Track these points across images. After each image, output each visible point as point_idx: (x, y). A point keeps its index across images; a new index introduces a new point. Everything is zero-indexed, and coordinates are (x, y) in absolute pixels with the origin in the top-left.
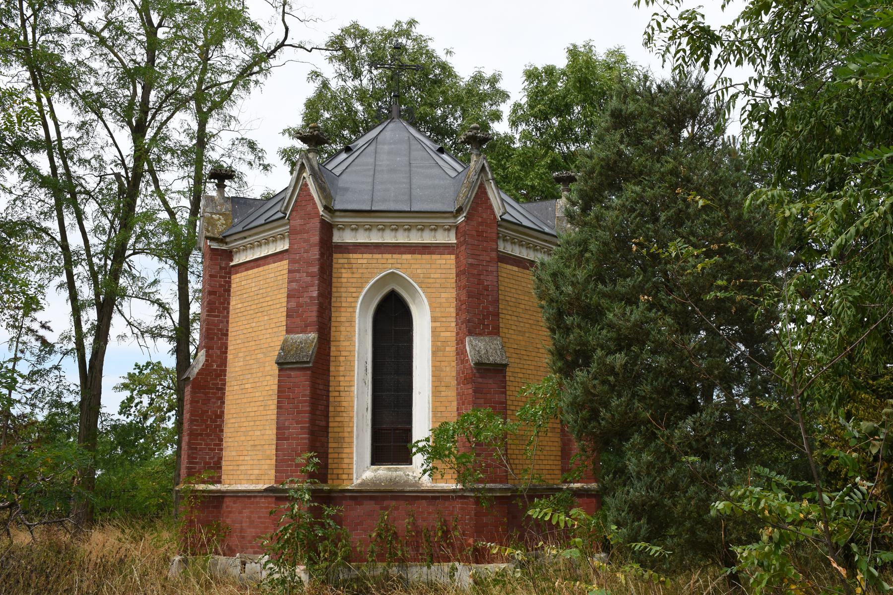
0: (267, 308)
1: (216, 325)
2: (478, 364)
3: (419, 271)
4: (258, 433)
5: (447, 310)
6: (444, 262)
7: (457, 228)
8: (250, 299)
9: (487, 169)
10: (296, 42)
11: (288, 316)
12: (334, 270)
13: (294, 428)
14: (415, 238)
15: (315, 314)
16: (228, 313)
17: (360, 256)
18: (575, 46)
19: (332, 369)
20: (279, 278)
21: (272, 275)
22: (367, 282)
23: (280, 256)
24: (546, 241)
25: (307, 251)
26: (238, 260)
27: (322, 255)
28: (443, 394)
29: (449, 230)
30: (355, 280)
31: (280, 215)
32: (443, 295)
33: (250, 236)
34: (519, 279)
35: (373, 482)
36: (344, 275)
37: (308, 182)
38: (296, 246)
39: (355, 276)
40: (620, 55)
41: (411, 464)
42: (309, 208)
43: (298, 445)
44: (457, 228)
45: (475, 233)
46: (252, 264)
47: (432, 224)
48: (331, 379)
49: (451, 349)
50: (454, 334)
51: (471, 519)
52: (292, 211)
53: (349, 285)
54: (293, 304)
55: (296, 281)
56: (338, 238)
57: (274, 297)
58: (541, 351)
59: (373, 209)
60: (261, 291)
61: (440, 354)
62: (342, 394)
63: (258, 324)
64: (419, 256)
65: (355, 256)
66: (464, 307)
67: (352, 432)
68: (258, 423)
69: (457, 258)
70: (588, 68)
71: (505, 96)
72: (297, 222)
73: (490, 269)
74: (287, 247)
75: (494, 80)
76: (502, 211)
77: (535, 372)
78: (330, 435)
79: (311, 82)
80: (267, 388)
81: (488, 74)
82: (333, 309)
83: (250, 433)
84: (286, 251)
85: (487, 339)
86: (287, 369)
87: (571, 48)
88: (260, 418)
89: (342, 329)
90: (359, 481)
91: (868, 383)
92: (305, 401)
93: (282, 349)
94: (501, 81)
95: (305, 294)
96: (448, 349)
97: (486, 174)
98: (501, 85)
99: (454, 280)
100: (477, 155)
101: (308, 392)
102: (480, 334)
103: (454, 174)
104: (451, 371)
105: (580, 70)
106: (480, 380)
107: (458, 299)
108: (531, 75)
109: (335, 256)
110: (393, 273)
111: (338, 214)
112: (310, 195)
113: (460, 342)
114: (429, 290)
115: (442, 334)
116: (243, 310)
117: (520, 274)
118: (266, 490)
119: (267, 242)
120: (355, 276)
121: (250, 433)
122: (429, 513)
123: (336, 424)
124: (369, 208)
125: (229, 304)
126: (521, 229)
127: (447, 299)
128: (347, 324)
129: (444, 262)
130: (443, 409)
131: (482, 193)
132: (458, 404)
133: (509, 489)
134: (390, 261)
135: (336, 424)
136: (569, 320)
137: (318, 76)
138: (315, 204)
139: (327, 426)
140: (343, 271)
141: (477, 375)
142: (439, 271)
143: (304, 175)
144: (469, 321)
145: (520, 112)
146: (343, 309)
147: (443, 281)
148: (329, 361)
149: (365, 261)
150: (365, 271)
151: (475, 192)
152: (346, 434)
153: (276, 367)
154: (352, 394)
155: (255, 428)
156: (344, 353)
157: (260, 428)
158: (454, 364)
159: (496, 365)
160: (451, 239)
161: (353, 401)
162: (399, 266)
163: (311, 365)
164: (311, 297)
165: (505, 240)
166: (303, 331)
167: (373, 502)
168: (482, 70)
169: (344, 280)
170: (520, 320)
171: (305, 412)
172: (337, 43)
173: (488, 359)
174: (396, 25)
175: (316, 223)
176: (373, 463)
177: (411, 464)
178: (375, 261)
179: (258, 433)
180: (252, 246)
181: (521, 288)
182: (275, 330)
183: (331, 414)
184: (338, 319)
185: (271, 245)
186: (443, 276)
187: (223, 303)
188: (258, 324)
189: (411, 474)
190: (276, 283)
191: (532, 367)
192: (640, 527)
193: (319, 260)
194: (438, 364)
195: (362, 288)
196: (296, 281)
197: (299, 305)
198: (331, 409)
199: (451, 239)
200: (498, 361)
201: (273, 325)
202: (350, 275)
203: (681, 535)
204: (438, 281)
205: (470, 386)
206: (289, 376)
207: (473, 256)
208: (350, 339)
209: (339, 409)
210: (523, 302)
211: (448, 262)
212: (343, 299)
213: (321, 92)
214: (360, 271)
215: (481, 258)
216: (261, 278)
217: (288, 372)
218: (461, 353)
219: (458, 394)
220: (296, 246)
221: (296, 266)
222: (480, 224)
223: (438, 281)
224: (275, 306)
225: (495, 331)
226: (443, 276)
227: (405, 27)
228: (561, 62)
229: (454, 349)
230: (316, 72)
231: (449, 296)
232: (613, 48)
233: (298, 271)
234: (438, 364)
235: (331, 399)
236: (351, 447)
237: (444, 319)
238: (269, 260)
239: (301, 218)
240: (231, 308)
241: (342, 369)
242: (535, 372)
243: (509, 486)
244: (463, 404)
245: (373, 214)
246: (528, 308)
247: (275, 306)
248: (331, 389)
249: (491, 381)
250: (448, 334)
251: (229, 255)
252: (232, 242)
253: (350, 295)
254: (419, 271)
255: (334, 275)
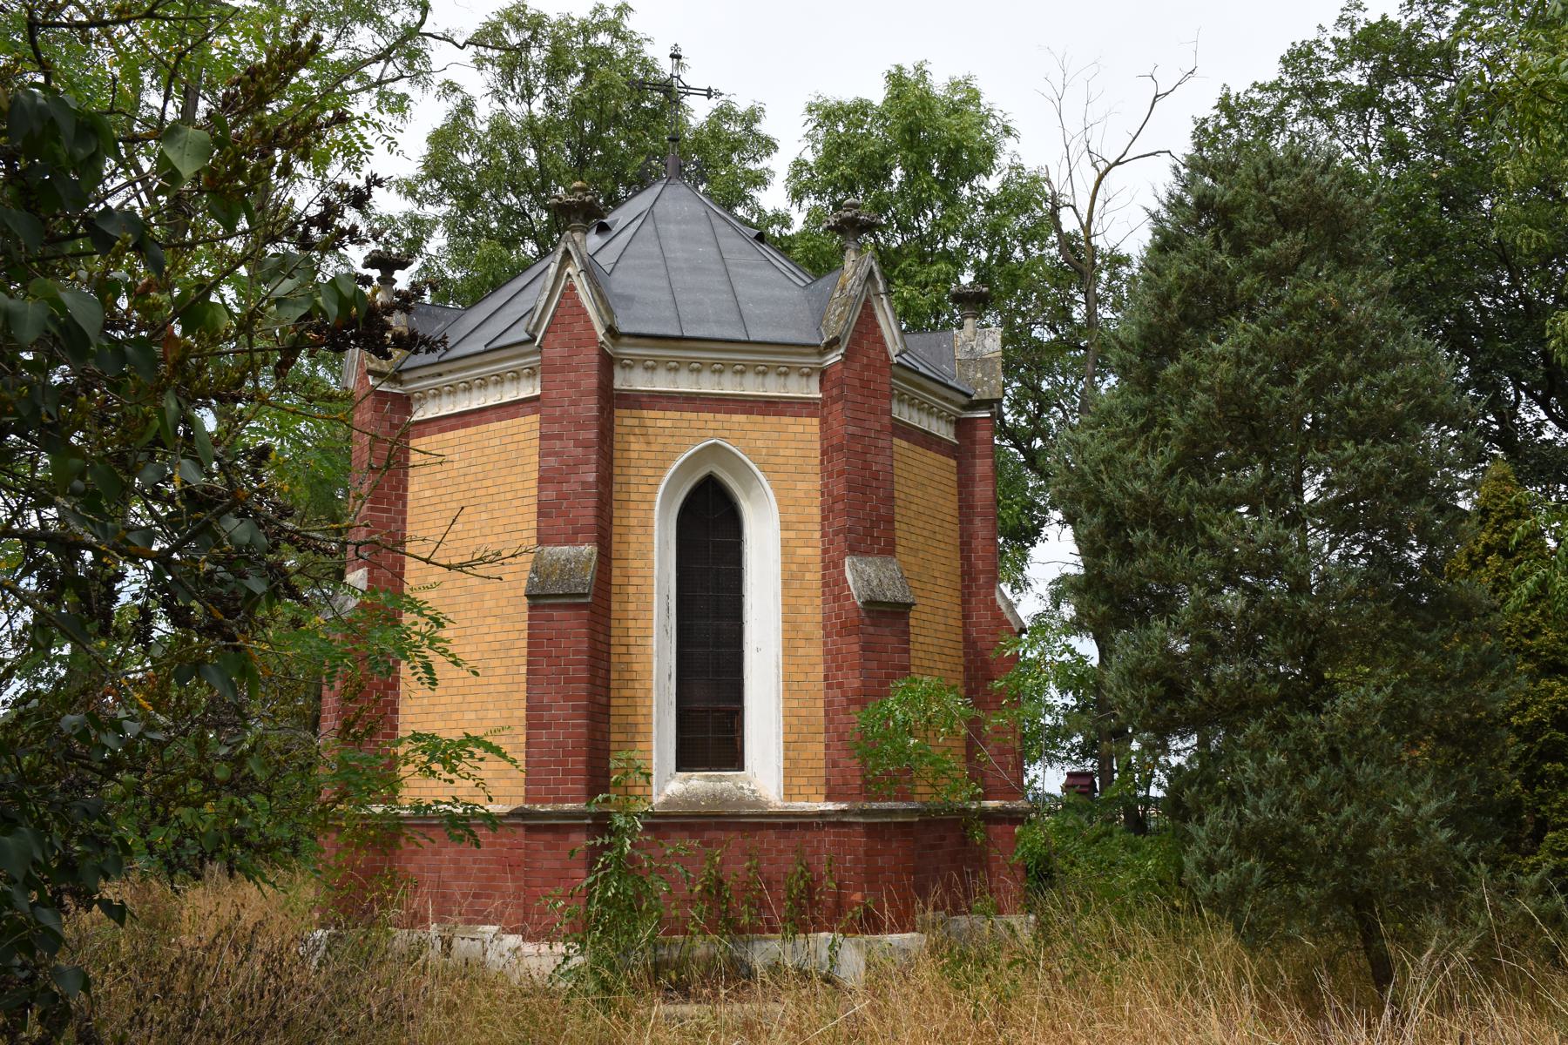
0: (484, 500)
1: (384, 526)
2: (870, 603)
3: (759, 443)
4: (472, 716)
5: (807, 510)
6: (801, 429)
7: (823, 373)
8: (450, 482)
9: (878, 276)
10: (438, 31)
11: (540, 514)
12: (616, 438)
13: (560, 708)
14: (752, 387)
15: (591, 512)
16: (405, 505)
17: (660, 414)
18: (900, 68)
19: (615, 606)
20: (510, 447)
21: (497, 441)
22: (673, 460)
23: (512, 410)
24: (946, 399)
25: (574, 403)
26: (425, 412)
27: (601, 409)
28: (801, 652)
29: (808, 375)
30: (652, 456)
31: (519, 334)
32: (800, 485)
33: (450, 372)
34: (910, 461)
35: (685, 799)
36: (633, 447)
37: (577, 284)
38: (554, 394)
39: (654, 448)
40: (970, 90)
41: (741, 768)
42: (578, 328)
43: (567, 736)
44: (823, 373)
45: (857, 383)
46: (453, 421)
47: (740, 362)
48: (614, 623)
49: (814, 577)
50: (819, 551)
51: (857, 861)
52: (546, 332)
53: (642, 463)
54: (550, 494)
55: (556, 454)
56: (622, 381)
57: (500, 481)
58: (939, 582)
59: (686, 334)
60: (473, 469)
61: (796, 584)
62: (633, 650)
63: (468, 526)
64: (760, 418)
65: (652, 414)
66: (839, 506)
67: (649, 715)
68: (470, 698)
69: (824, 422)
70: (923, 109)
71: (769, 146)
72: (556, 352)
73: (880, 443)
74: (538, 392)
75: (752, 117)
76: (900, 346)
77: (931, 617)
78: (613, 720)
79: (443, 100)
80: (488, 638)
81: (742, 107)
82: (615, 504)
83: (455, 716)
84: (537, 398)
85: (878, 560)
86: (544, 606)
87: (894, 71)
88: (474, 690)
89: (632, 538)
90: (662, 799)
91: (1522, 644)
92: (580, 662)
93: (535, 571)
94: (763, 120)
95: (573, 478)
96: (808, 576)
97: (875, 283)
98: (764, 128)
99: (817, 461)
100: (856, 251)
101: (584, 647)
102: (866, 553)
103: (803, 284)
104: (813, 613)
105: (911, 113)
106: (871, 630)
107: (825, 491)
108: (828, 114)
109: (617, 412)
110: (715, 445)
111: (625, 340)
112: (578, 305)
113: (831, 566)
114: (777, 476)
115: (800, 551)
116: (434, 500)
117: (910, 454)
118: (511, 814)
119: (484, 383)
120: (654, 448)
121: (455, 716)
122: (780, 852)
123: (622, 702)
124: (677, 333)
125: (405, 489)
126: (916, 378)
127: (807, 492)
128: (640, 530)
129: (801, 429)
130: (802, 677)
131: (867, 320)
132: (828, 669)
133: (917, 810)
134: (712, 425)
135: (622, 702)
136: (1137, 537)
137: (455, 90)
138: (588, 321)
139: (608, 706)
140: (632, 438)
141: (867, 621)
142: (793, 445)
143: (569, 270)
144: (850, 531)
145: (806, 176)
146: (632, 505)
147: (800, 461)
148: (609, 592)
149: (669, 424)
150: (669, 440)
151: (858, 314)
152: (641, 719)
153: (526, 600)
154: (649, 651)
155: (465, 707)
156: (634, 581)
157: (473, 707)
158: (819, 601)
159: (897, 604)
160: (813, 391)
161: (650, 663)
162: (726, 433)
163: (589, 600)
164: (583, 483)
165: (901, 401)
166: (571, 540)
167: (686, 834)
168: (732, 99)
169: (634, 455)
170: (912, 529)
171: (579, 680)
172: (487, 36)
173: (886, 596)
174: (596, 11)
175: (592, 355)
176: (678, 769)
177: (741, 768)
178: (685, 424)
179: (472, 716)
180: (453, 390)
181: (912, 477)
182: (502, 537)
183: (613, 684)
184: (625, 522)
185: (491, 389)
186: (800, 453)
187: (396, 488)
188: (468, 526)
189: (746, 786)
190: (503, 456)
191: (927, 609)
192: (1251, 870)
193: (598, 419)
194: (793, 601)
195: (665, 468)
196: (556, 454)
197: (562, 496)
198: (614, 675)
199: (813, 391)
200: (900, 598)
201: (500, 530)
202: (644, 447)
203: (1324, 881)
204: (791, 461)
205: (853, 638)
206: (550, 619)
207: (856, 421)
208: (645, 555)
209: (627, 676)
210: (916, 500)
211: (808, 429)
212: (633, 488)
213: (456, 119)
214: (660, 439)
215: (867, 425)
216: (473, 446)
217: (547, 612)
218: (833, 584)
219: (827, 652)
220: (554, 394)
221: (556, 428)
222: (867, 367)
223: (791, 461)
224: (502, 497)
225: (889, 549)
226: (800, 453)
227: (611, 15)
228: (877, 94)
229: (819, 576)
230: (452, 84)
231: (810, 486)
232: (960, 77)
233: (559, 437)
234: (793, 601)
235: (614, 659)
236: (649, 741)
237: (802, 526)
238: (488, 415)
239: (563, 345)
240: (410, 496)
241: (632, 607)
242: (931, 617)
243: (915, 805)
244: (839, 668)
245: (684, 344)
246: (921, 510)
247: (502, 497)
248: (613, 641)
249: (887, 631)
250: (809, 551)
251: (405, 403)
252: (412, 381)
253: (643, 480)
254: (759, 443)
255: (617, 446)
